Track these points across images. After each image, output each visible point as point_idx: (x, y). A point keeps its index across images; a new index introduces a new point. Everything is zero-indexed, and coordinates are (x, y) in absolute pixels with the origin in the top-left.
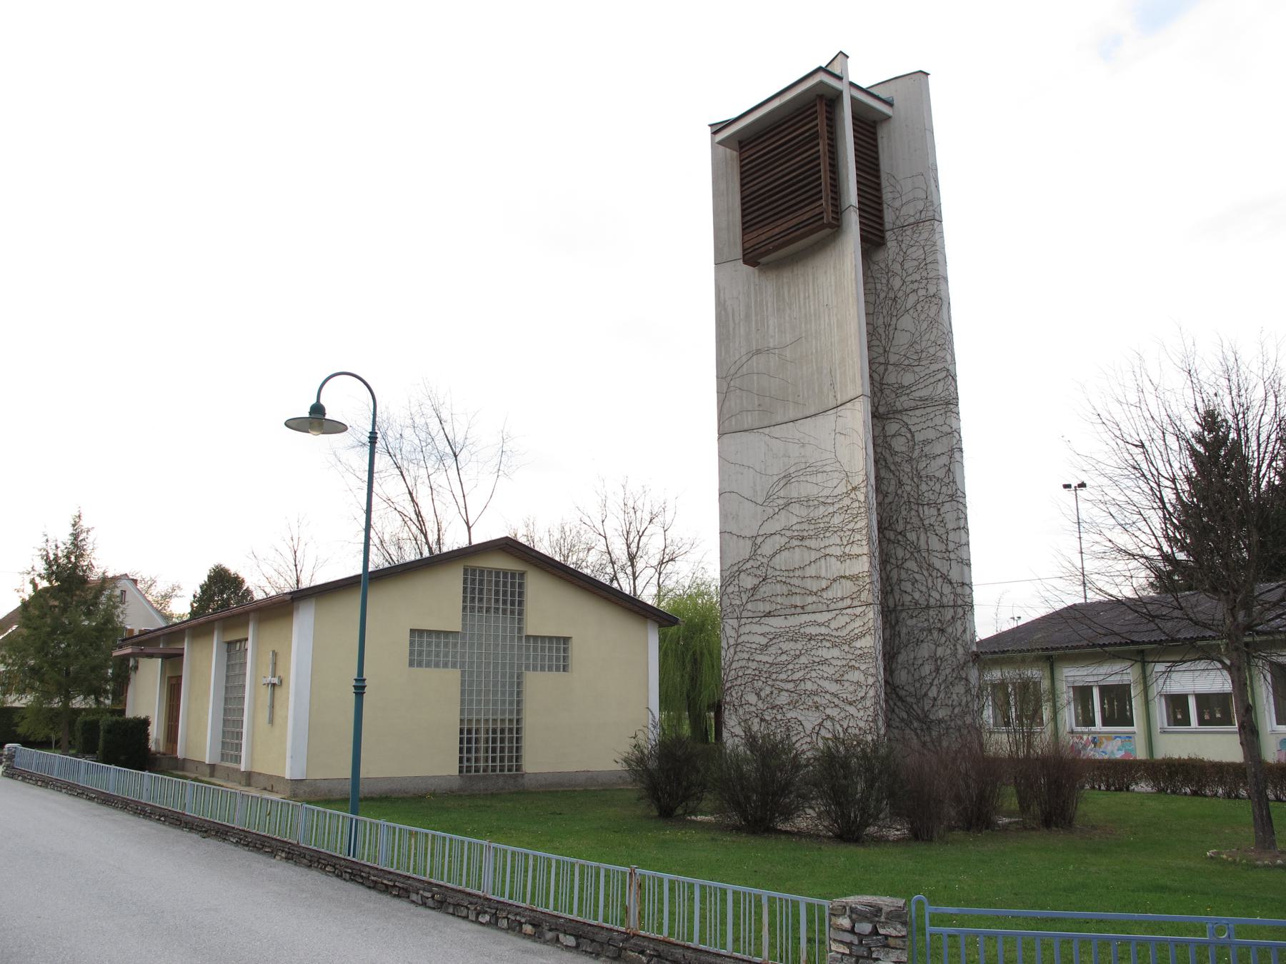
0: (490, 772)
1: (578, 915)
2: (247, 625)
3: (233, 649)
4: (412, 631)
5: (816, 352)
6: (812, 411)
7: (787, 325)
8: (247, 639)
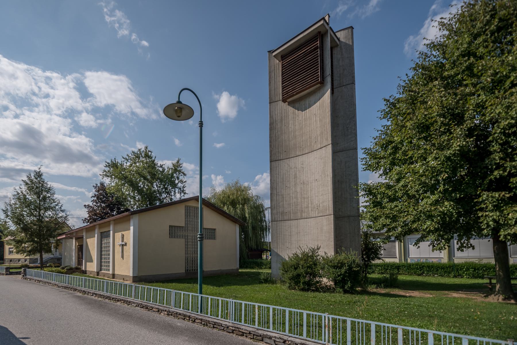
0: (193, 271)
1: (303, 313)
2: (109, 226)
3: (104, 235)
4: (170, 226)
5: (309, 131)
6: (307, 152)
7: (297, 123)
8: (110, 231)
